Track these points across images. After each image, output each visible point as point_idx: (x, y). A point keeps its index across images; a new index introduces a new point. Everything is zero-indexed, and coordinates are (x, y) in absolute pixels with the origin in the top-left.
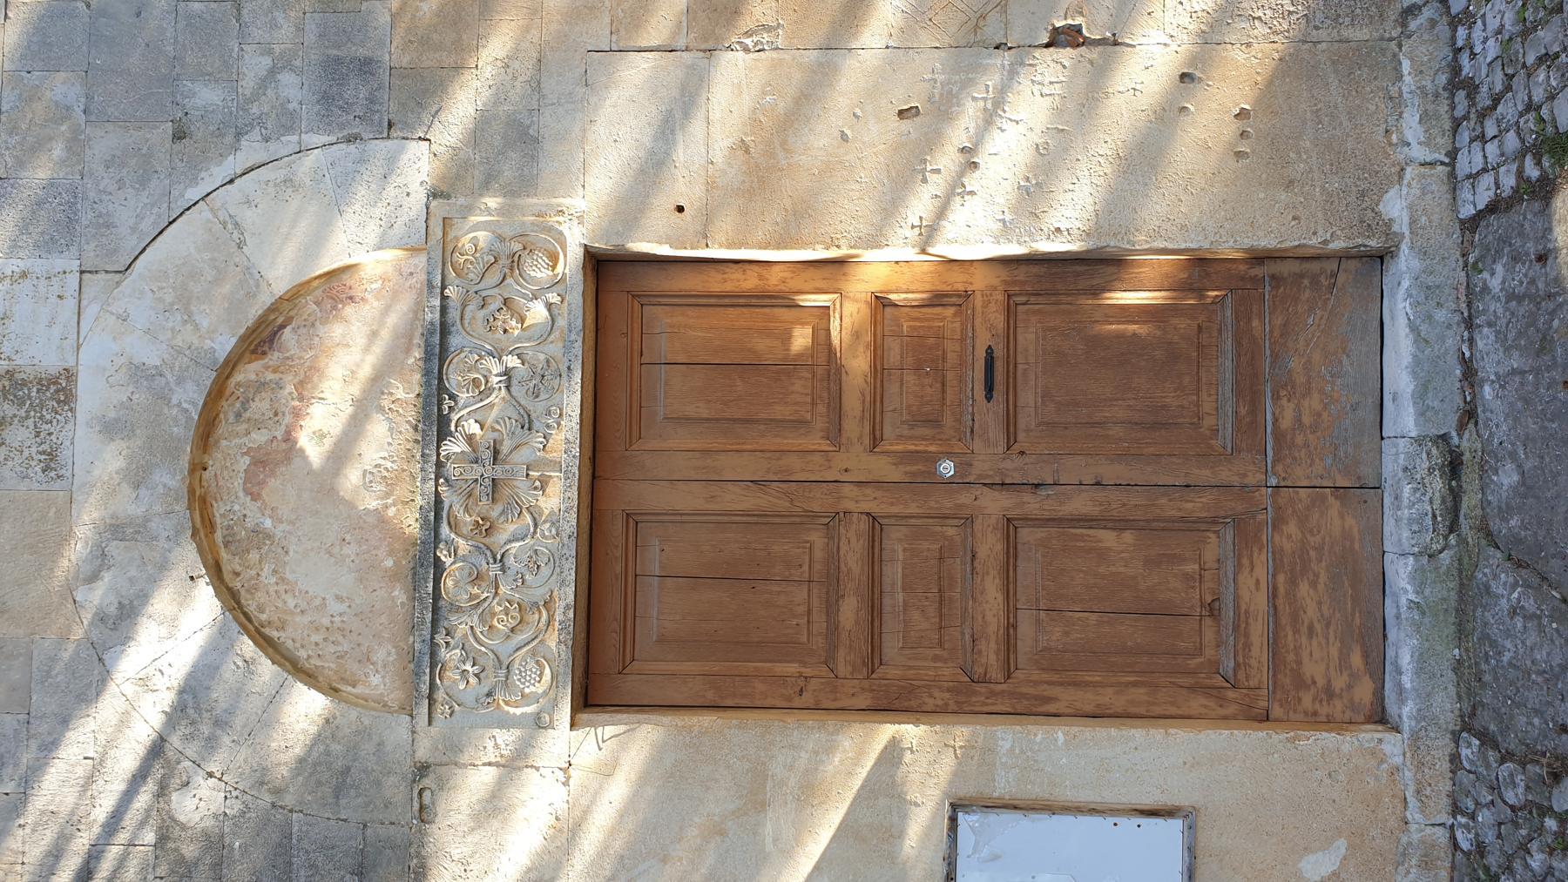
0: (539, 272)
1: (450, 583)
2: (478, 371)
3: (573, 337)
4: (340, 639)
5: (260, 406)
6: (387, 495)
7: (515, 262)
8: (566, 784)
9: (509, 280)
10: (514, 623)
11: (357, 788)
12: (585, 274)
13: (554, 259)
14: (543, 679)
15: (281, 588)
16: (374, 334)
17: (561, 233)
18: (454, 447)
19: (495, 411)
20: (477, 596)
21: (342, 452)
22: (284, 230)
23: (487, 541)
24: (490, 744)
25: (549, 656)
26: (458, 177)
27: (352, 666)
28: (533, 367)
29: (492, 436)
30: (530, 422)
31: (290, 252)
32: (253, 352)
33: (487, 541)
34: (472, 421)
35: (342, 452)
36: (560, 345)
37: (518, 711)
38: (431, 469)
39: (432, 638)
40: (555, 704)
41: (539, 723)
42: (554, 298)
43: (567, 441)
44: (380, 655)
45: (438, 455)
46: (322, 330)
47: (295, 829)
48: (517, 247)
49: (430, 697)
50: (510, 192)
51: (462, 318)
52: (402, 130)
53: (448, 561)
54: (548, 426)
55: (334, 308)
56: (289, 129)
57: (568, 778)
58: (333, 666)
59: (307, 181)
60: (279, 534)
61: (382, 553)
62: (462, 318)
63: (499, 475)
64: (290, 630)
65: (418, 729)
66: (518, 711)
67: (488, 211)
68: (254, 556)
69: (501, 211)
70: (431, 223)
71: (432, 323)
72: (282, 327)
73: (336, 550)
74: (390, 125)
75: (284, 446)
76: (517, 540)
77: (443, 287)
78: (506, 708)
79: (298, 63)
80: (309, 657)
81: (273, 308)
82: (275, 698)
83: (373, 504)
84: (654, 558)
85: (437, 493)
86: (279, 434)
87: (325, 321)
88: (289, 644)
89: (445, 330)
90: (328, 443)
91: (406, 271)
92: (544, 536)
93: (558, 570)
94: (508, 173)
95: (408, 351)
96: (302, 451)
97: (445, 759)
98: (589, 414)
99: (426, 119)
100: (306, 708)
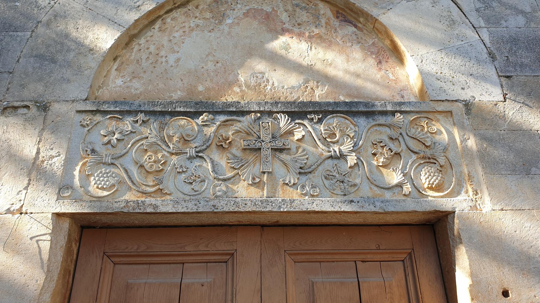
0: (426, 178)
1: (183, 122)
2: (342, 136)
3: (378, 204)
4: (150, 61)
5: (304, 16)
6: (248, 87)
7: (430, 160)
8: (8, 211)
9: (414, 157)
10: (147, 167)
11: (40, 68)
12: (430, 213)
13: (438, 188)
14: (101, 190)
15: (187, 29)
16: (358, 76)
17: (459, 193)
18: (283, 121)
19: (312, 149)
20: (170, 141)
21: (277, 60)
22: (421, 20)
23: (214, 146)
24: (53, 153)
25: (117, 195)
26: (484, 120)
27: (130, 69)
28: (349, 174)
29: (293, 147)
30: (305, 174)
31: (407, 23)
32: (338, 12)
33: (214, 146)
34: (303, 133)
35: (277, 60)
36: (370, 194)
37: (76, 173)
38: (267, 108)
39: (142, 112)
40: (77, 200)
41: (64, 188)
42: (407, 188)
43: (292, 201)
44: (136, 84)
45: (278, 112)
46: (357, 47)
47: (20, 34)
48: (442, 160)
49: (97, 112)
50: (483, 156)
51: (380, 125)
52: (507, 83)
53: (199, 121)
54: (303, 187)
55: (372, 53)
56: (488, 21)
57: (13, 213)
58: (132, 58)
59: (456, 32)
60: (221, 27)
61: (208, 84)
62: (380, 125)
63: (263, 153)
64: (159, 34)
65: (75, 104)
66: (76, 173)
67: (464, 140)
68: (208, 15)
69: (466, 150)
70: (446, 103)
71: (373, 105)
72: (356, 26)
73: (211, 58)
74: (508, 77)
75: (279, 29)
76: (213, 167)
77: (401, 112)
78: (81, 164)
79: (533, 25)
80: (140, 45)
81: (367, 16)
82: (112, 22)
83: (242, 79)
84: (197, 277)
85: (249, 112)
86: (287, 26)
87: (363, 48)
88: (149, 34)
89: (369, 114)
90: (283, 52)
91: (405, 93)
92: (215, 186)
93: (188, 198)
94: (497, 153)
95: (349, 95)
96: (277, 38)
97: (48, 121)
98: (314, 220)
99: (520, 98)
100: (104, 38)
